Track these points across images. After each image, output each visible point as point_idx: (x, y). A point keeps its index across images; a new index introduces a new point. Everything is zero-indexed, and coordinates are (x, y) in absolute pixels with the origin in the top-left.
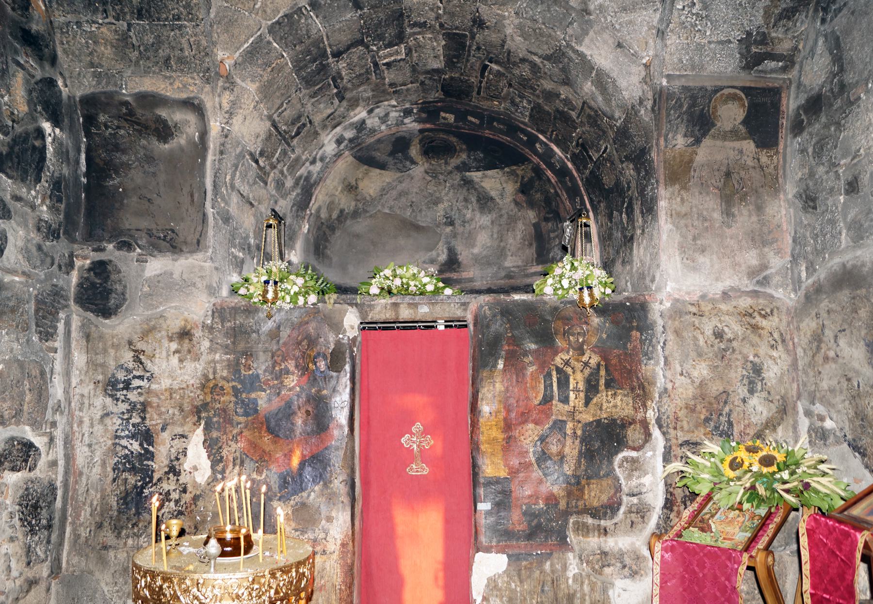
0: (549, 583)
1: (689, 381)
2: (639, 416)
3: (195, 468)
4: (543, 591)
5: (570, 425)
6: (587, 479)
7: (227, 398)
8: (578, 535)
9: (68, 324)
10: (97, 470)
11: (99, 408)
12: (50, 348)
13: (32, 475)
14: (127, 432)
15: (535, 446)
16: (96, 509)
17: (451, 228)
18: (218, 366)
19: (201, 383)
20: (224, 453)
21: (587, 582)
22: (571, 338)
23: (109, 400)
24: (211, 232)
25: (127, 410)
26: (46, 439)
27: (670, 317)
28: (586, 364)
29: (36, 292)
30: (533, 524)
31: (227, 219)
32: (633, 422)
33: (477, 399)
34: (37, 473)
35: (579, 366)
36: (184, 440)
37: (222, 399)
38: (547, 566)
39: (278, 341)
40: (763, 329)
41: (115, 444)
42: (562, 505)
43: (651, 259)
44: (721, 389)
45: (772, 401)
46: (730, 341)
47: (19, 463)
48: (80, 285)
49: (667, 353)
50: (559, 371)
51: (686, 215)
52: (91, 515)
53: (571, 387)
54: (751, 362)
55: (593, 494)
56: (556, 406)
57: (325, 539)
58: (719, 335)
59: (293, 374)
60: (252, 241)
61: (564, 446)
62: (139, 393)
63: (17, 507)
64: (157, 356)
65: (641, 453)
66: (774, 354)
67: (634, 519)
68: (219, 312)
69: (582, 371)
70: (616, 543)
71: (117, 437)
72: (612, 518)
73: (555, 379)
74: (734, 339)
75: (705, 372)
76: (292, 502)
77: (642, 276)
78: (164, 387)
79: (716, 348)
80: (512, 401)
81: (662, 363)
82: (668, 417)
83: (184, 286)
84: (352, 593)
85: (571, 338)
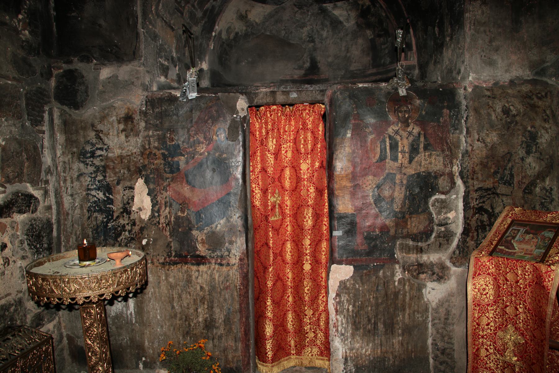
0: (382, 285)
1: (484, 145)
2: (447, 170)
3: (140, 209)
4: (377, 290)
5: (398, 177)
6: (410, 214)
7: (159, 162)
8: (403, 253)
9: (51, 114)
10: (78, 211)
11: (76, 170)
12: (39, 130)
13: (34, 215)
14: (95, 186)
15: (374, 191)
16: (79, 237)
17: (312, 44)
18: (152, 140)
19: (141, 152)
20: (159, 199)
21: (407, 284)
22: (400, 114)
23: (82, 165)
24: (142, 46)
25: (94, 171)
26: (42, 192)
27: (472, 99)
28: (410, 133)
29: (25, 92)
30: (372, 245)
31: (155, 37)
32: (443, 174)
33: (332, 159)
34: (38, 214)
35: (405, 134)
36: (132, 190)
37: (155, 162)
38: (381, 273)
39: (192, 121)
40: (539, 107)
41: (87, 194)
42: (392, 232)
43: (457, 57)
44: (506, 151)
45: (542, 160)
46: (514, 116)
47: (24, 208)
48: (57, 87)
49: (469, 125)
50: (390, 137)
51: (484, 23)
52: (76, 241)
53: (400, 150)
54: (529, 131)
55: (413, 225)
56: (389, 163)
57: (228, 256)
58: (506, 111)
59: (203, 143)
60: (174, 55)
61: (394, 191)
62: (101, 160)
63: (25, 237)
64: (111, 134)
65: (448, 196)
66: (546, 126)
67: (441, 241)
68: (151, 102)
69: (407, 138)
70: (429, 258)
71: (89, 189)
72: (426, 241)
73: (388, 144)
74: (517, 115)
75: (495, 139)
76: (205, 231)
77: (450, 71)
78: (116, 155)
79: (504, 122)
80: (358, 160)
81: (465, 132)
82: (468, 171)
83: (128, 85)
84: (247, 292)
85: (400, 114)
